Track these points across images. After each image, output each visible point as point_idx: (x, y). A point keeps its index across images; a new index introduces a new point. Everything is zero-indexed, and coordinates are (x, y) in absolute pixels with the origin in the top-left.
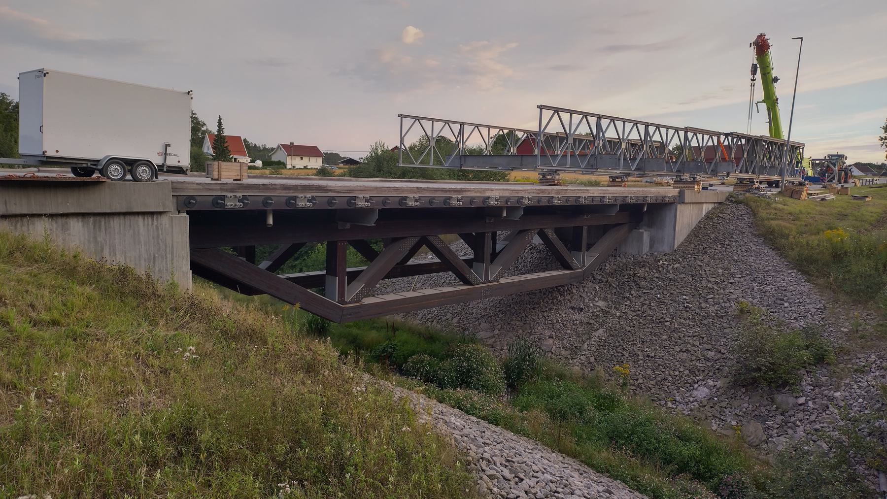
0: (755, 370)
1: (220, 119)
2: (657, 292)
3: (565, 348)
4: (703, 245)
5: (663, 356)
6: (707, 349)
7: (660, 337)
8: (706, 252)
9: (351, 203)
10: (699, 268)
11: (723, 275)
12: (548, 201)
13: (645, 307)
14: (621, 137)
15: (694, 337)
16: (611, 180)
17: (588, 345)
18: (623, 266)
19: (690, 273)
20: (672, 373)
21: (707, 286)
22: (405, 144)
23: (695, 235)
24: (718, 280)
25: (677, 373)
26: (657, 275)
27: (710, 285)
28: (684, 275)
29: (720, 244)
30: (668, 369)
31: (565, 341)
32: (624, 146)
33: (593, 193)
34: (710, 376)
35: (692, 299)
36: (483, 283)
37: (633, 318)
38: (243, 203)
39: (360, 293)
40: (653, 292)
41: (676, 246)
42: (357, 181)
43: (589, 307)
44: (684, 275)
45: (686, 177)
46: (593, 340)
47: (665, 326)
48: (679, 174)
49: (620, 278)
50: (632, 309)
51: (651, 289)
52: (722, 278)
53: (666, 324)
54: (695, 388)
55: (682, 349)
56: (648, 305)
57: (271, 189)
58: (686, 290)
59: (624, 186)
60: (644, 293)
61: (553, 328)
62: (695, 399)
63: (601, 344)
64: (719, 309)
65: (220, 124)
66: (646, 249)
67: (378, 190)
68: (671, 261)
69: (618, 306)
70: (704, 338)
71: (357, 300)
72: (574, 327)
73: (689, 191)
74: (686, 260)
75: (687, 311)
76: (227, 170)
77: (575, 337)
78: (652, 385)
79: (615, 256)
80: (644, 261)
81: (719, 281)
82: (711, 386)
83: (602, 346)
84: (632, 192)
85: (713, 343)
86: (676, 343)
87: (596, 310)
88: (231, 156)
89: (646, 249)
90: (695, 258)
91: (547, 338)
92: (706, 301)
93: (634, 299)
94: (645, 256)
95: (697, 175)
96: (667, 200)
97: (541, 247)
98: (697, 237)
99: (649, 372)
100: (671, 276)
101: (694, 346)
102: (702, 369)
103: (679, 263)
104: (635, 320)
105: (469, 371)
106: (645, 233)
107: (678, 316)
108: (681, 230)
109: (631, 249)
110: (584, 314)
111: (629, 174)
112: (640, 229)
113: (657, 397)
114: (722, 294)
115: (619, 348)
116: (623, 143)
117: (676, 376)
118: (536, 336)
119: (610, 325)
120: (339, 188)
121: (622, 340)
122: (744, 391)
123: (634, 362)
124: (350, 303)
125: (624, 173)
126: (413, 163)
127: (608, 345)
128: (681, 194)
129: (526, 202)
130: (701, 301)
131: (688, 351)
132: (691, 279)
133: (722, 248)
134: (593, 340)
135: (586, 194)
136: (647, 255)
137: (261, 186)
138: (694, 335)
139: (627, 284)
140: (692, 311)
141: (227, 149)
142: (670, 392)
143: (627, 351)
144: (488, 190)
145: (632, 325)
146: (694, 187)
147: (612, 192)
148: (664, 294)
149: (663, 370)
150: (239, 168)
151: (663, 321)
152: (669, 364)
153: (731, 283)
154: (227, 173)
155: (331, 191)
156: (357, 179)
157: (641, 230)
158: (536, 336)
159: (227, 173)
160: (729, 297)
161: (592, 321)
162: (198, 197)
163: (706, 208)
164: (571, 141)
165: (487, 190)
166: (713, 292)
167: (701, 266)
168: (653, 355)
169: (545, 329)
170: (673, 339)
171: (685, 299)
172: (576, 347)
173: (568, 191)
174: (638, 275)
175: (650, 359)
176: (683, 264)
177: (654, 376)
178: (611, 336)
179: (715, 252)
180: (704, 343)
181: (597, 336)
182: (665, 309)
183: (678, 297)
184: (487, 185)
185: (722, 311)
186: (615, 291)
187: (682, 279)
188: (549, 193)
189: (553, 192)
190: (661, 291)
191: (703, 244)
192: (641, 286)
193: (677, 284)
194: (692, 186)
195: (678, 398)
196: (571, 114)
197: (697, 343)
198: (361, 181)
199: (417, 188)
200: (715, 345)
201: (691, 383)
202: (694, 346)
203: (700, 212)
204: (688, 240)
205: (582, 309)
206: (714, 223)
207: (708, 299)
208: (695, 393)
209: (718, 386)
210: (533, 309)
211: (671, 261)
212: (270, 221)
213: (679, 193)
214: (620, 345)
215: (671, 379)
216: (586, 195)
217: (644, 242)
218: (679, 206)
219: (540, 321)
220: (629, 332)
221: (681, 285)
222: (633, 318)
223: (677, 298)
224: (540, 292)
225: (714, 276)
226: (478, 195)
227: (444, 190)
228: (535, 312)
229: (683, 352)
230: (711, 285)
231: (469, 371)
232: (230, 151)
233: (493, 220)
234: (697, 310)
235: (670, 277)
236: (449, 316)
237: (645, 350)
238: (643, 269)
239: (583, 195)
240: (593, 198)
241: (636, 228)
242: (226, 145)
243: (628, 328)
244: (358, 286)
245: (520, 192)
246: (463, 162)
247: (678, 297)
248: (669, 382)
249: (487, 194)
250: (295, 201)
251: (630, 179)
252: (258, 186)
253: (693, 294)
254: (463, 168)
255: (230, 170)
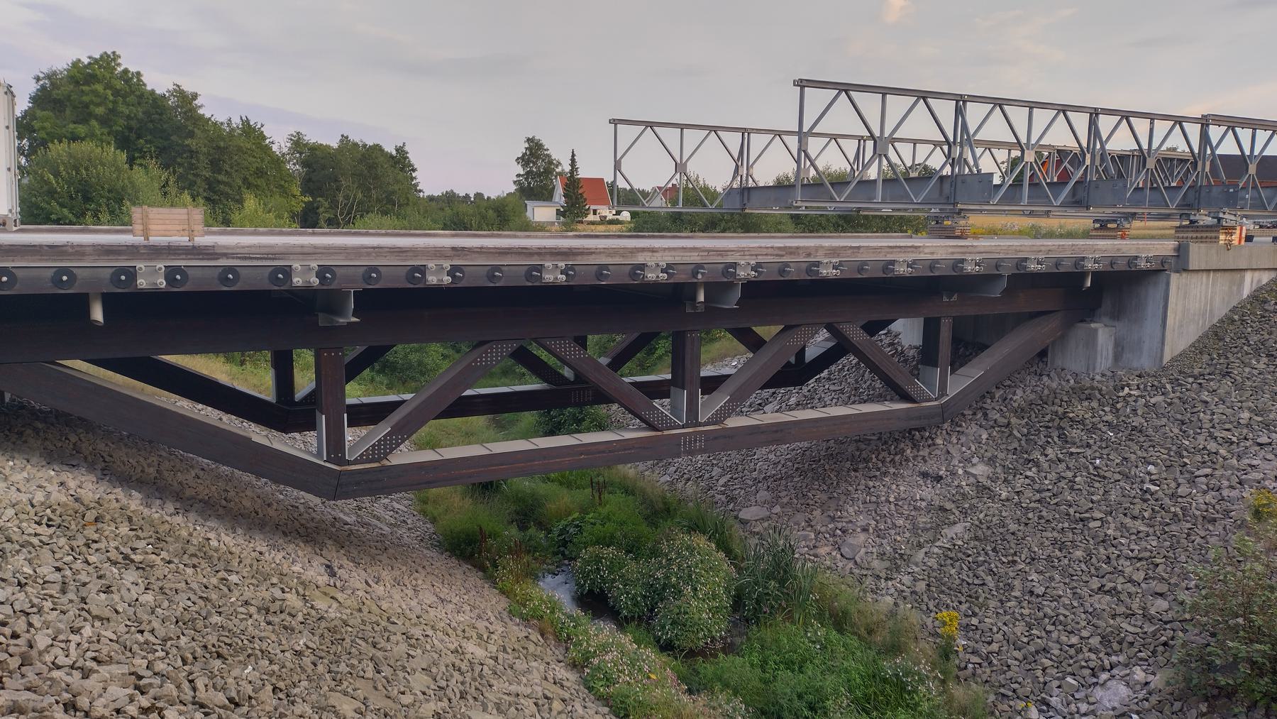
0: (1224, 669)
1: (573, 155)
2: (1097, 454)
3: (882, 556)
4: (1227, 358)
5: (1060, 597)
6: (1156, 594)
7: (1069, 553)
8: (1231, 372)
9: (811, 270)
10: (1200, 407)
11: (1248, 426)
12: (1129, 264)
13: (1063, 484)
14: (1145, 146)
15: (1140, 560)
16: (1097, 225)
17: (926, 553)
18: (1048, 396)
19: (1179, 417)
20: (1064, 639)
21: (1205, 448)
22: (754, 176)
23: (1216, 335)
24: (1233, 435)
25: (1074, 640)
26: (1109, 417)
27: (1212, 446)
28: (1164, 421)
29: (1268, 356)
30: (1060, 627)
31: (886, 540)
32: (1252, 169)
33: (932, 253)
34: (1141, 659)
35: (1164, 475)
36: (683, 427)
37: (1033, 505)
38: (667, 273)
39: (379, 445)
40: (1089, 452)
41: (1167, 358)
42: (528, 237)
43: (954, 474)
44: (1164, 421)
45: (1205, 219)
46: (937, 544)
47: (1089, 529)
48: (1186, 212)
49: (1036, 420)
50: (1037, 487)
51: (1089, 446)
52: (1245, 431)
53: (1092, 524)
54: (1101, 681)
55: (1103, 586)
56: (1070, 481)
57: (71, 254)
58: (1158, 454)
59: (1122, 237)
60: (1072, 454)
61: (876, 512)
62: (1092, 707)
63: (952, 556)
64: (1213, 502)
65: (573, 160)
66: (1104, 360)
67: (347, 253)
68: (1149, 388)
69: (1011, 477)
70: (1157, 565)
71: (373, 457)
72: (913, 513)
73: (1201, 245)
74: (1179, 388)
75: (1145, 501)
76: (161, 222)
77: (907, 535)
78: (1016, 659)
79: (1041, 375)
80: (1092, 388)
81: (1234, 439)
82: (1138, 683)
83: (951, 558)
84: (1043, 248)
85: (1172, 581)
86: (1097, 569)
87: (964, 483)
88: (587, 207)
89: (1104, 360)
90: (1200, 384)
91: (859, 530)
92: (1192, 481)
93: (1046, 466)
94: (1098, 378)
95: (1224, 213)
96: (1143, 265)
97: (912, 353)
98: (1220, 340)
99: (1020, 628)
100: (1137, 421)
101: (1131, 581)
102: (1130, 638)
103: (1163, 394)
104: (1034, 510)
105: (664, 587)
106: (1100, 332)
107: (1121, 510)
108: (1181, 326)
109: (1072, 360)
110: (941, 488)
111: (1135, 214)
112: (1092, 321)
113: (1014, 691)
114: (1232, 467)
115: (981, 568)
116: (1250, 166)
117: (1071, 646)
118: (840, 525)
119: (981, 516)
120: (246, 251)
121: (994, 550)
122: (1204, 710)
123: (1001, 601)
124: (356, 462)
125: (1124, 213)
126: (705, 206)
127: (964, 557)
128: (1181, 252)
129: (742, 274)
130: (1180, 481)
131: (1113, 592)
132: (1176, 431)
133: (1268, 365)
134: (937, 544)
135: (910, 255)
136: (1103, 375)
137: (46, 248)
138: (1139, 556)
139: (1043, 432)
140: (1157, 500)
141: (582, 197)
142: (1045, 683)
143: (995, 575)
144: (643, 250)
145: (1023, 520)
146: (1217, 238)
147: (987, 249)
148: (1109, 459)
149: (1049, 628)
150: (185, 217)
151: (1088, 518)
152: (1066, 617)
153: (1260, 445)
154: (159, 227)
155: (226, 255)
156: (527, 233)
157: (1093, 325)
158: (840, 525)
159: (159, 227)
160: (1244, 477)
161: (948, 505)
162: (76, 269)
163: (1249, 283)
164: (1151, 164)
165: (638, 252)
166: (1214, 463)
167: (1206, 402)
168: (1040, 590)
169: (861, 512)
170: (1094, 560)
171: (1149, 474)
172: (901, 555)
173: (861, 250)
174: (1071, 415)
175: (1033, 599)
176: (1172, 395)
177: (1025, 640)
178: (976, 538)
179: (1249, 373)
180: (1153, 579)
181: (949, 536)
182: (1101, 492)
183: (1137, 467)
184: (809, 240)
185: (1217, 507)
186: (1016, 445)
187: (1156, 429)
188: (809, 255)
189: (821, 252)
190: (1105, 451)
191: (1229, 355)
192: (1069, 439)
193: (1142, 439)
194: (1213, 235)
195: (1054, 701)
196: (884, 95)
197: (1139, 576)
198: (536, 237)
199: (454, 249)
200: (1176, 585)
201: (1096, 670)
202: (1131, 581)
203: (1235, 288)
204: (1199, 348)
205: (939, 479)
206: (1266, 311)
207: (1196, 477)
208: (1098, 693)
209: (1152, 686)
210: (855, 470)
211: (1149, 388)
212: (98, 314)
213: (1178, 249)
214: (985, 561)
215: (1056, 652)
216: (910, 257)
217: (1099, 348)
218: (1174, 278)
219: (857, 496)
220: (1013, 534)
221: (1150, 441)
222: (1033, 505)
223: (1133, 470)
224: (880, 439)
225: (1227, 426)
226: (617, 260)
227: (524, 251)
228: (856, 477)
229: (1106, 592)
230: (1215, 445)
231: (664, 587)
232: (585, 200)
233: (956, 296)
234: (1167, 501)
235: (1133, 424)
236: (716, 471)
237: (1030, 578)
238: (1086, 403)
239: (900, 257)
240: (933, 264)
241: (1082, 321)
242: (580, 191)
243: (1013, 527)
244: (721, 399)
245: (729, 253)
246: (746, 202)
247: (1137, 467)
248: (1051, 659)
249: (640, 259)
250: (540, 272)
251: (1136, 224)
252: (38, 248)
253: (1168, 463)
254: (747, 211)
255: (167, 222)
